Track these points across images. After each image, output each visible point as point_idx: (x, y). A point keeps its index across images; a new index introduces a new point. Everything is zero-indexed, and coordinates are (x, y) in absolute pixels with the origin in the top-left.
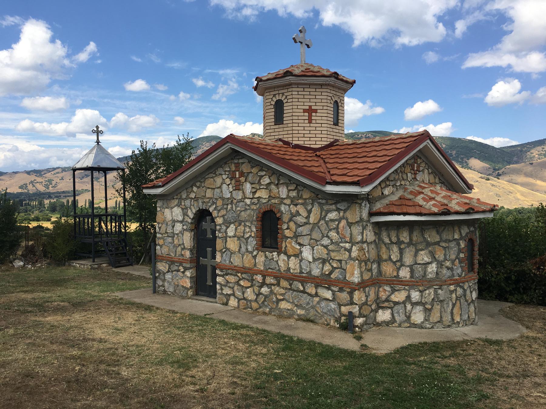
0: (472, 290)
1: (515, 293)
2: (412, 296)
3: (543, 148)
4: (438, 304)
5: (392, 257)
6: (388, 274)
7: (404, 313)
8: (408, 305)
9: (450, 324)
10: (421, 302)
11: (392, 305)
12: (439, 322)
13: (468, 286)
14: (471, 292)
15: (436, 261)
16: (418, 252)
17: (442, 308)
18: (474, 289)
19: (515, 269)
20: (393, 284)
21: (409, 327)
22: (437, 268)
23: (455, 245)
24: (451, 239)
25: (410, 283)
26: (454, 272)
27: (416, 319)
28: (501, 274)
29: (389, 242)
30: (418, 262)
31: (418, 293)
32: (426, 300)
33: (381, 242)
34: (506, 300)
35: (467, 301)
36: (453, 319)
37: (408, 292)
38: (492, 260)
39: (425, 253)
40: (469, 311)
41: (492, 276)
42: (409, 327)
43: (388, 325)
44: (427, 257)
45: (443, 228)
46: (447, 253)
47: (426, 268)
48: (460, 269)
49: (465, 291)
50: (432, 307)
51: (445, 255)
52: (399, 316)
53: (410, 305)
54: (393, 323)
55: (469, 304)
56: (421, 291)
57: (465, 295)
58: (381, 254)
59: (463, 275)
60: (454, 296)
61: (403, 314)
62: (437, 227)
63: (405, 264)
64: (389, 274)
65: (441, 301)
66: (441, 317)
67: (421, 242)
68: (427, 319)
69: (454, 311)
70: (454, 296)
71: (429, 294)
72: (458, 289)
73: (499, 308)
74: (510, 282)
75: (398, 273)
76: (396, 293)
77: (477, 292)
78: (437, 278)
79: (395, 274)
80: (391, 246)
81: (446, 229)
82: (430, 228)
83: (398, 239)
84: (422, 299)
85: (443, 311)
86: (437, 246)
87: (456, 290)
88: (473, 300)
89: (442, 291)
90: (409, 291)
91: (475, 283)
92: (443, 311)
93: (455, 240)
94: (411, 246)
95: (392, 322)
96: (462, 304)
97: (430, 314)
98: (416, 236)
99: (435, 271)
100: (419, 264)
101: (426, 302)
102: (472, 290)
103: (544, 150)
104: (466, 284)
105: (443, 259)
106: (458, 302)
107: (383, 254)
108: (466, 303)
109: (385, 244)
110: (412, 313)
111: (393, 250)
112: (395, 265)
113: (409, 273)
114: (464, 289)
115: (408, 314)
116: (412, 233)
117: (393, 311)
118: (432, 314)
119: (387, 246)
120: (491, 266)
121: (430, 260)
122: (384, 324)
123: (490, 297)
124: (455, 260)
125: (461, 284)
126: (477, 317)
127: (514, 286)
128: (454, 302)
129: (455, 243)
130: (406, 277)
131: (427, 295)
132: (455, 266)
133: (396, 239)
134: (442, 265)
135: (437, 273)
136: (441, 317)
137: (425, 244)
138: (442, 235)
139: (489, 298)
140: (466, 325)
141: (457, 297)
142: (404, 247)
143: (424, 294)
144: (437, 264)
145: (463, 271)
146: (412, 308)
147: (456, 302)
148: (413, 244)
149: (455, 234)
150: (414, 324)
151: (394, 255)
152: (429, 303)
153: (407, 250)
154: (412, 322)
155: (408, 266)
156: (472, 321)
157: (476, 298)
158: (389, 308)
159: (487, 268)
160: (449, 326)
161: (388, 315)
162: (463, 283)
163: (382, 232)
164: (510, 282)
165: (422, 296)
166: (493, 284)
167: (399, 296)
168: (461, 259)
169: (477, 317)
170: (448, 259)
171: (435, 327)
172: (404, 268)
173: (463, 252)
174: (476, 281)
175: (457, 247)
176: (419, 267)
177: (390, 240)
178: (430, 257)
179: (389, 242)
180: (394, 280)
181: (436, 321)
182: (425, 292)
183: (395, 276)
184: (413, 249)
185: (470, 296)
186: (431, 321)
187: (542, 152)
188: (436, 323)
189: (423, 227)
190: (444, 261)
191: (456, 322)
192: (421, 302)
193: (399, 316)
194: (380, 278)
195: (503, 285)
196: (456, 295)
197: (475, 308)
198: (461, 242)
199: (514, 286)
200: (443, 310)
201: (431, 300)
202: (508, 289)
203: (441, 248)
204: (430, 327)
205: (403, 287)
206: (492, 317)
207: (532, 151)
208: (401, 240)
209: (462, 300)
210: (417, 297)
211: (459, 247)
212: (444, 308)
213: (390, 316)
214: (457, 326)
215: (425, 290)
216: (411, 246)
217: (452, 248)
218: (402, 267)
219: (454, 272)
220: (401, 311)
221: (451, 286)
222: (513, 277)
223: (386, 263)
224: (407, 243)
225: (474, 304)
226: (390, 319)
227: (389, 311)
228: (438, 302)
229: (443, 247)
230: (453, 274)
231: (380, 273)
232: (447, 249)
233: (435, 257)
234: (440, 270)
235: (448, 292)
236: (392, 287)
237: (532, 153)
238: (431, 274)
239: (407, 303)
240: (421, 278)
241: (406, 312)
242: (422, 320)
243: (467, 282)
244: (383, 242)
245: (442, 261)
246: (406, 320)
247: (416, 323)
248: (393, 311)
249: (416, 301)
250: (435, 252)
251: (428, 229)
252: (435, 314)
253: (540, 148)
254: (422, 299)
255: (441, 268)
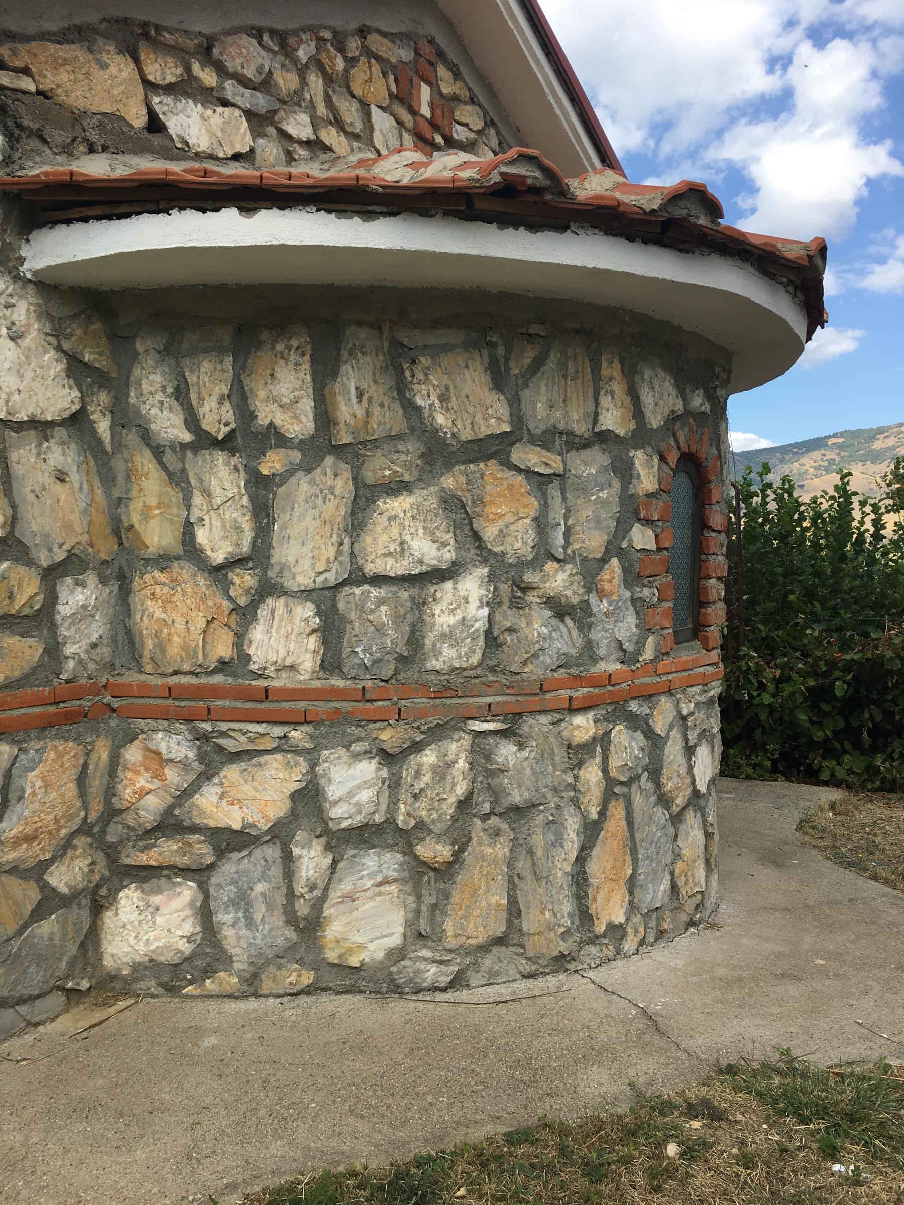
0: (692, 736)
1: (844, 751)
2: (333, 791)
3: (824, 455)
4: (497, 833)
5: (202, 536)
6: (174, 650)
7: (280, 899)
8: (308, 845)
9: (563, 947)
10: (390, 821)
11: (203, 851)
12: (500, 941)
13: (671, 717)
14: (689, 750)
15: (485, 561)
16: (371, 500)
17: (522, 853)
18: (703, 734)
19: (848, 657)
20: (209, 715)
21: (307, 991)
22: (494, 603)
23: (603, 470)
24: (581, 429)
25: (322, 707)
26: (596, 635)
27: (359, 939)
28: (795, 676)
29: (187, 437)
30: (370, 569)
31: (368, 769)
32: (422, 810)
33: (131, 438)
34: (812, 777)
35: (664, 800)
36: (585, 916)
37: (304, 766)
38: (761, 627)
39: (418, 507)
40: (677, 856)
41: (762, 687)
42: (307, 991)
43: (172, 990)
44: (431, 533)
45: (528, 356)
46: (557, 512)
47: (420, 605)
48: (631, 619)
49: (655, 742)
50: (457, 854)
51: (541, 524)
52: (249, 922)
53: (318, 847)
54: (208, 972)
55: (677, 819)
56: (388, 757)
57: (655, 771)
58: (135, 519)
59: (648, 654)
60: (592, 774)
61: (270, 908)
62: (492, 345)
63: (291, 585)
64: (185, 647)
65: (518, 812)
66: (514, 910)
67: (391, 438)
68: (424, 926)
69: (593, 867)
70: (592, 774)
71: (442, 771)
72: (620, 733)
73: (797, 816)
74: (825, 707)
75: (240, 639)
76: (231, 773)
77: (719, 749)
78: (493, 670)
79: (223, 648)
80: (195, 465)
81: (551, 364)
82: (446, 348)
83: (246, 414)
84: (394, 802)
85: (527, 873)
86: (491, 469)
87: (604, 740)
88: (696, 793)
89: (521, 746)
90: (312, 756)
91: (710, 703)
92: (527, 873)
93: (603, 438)
94: (329, 460)
95: (200, 963)
96: (638, 819)
97: (447, 896)
98: (360, 395)
99: (480, 625)
100: (378, 580)
101: (421, 826)
102: (692, 736)
103: (825, 458)
104: (665, 703)
105: (527, 552)
106: (617, 811)
107: (146, 516)
108: (661, 815)
109: (158, 452)
110: (335, 895)
111: (207, 493)
112: (225, 586)
113: (313, 642)
114: (649, 734)
115: (302, 909)
116: (335, 374)
117: (207, 896)
118: (456, 897)
119: (169, 458)
120: (756, 651)
121: (449, 555)
122: (151, 984)
123: (755, 766)
124: (604, 561)
125: (634, 706)
126: (715, 878)
127: (841, 724)
128: (594, 813)
129: (605, 460)
130: (292, 667)
131: (427, 778)
132: (601, 594)
133: (228, 413)
134: (526, 589)
135: (491, 640)
136: (514, 910)
137: (413, 447)
138: (526, 394)
139: (750, 771)
140: (661, 934)
141: (610, 782)
142: (279, 468)
143: (407, 775)
144: (492, 578)
145: (646, 629)
146: (335, 863)
147: (602, 813)
148: (339, 450)
149: (605, 401)
150: (341, 968)
151: (217, 523)
152: (438, 828)
153: (302, 486)
154: (332, 956)
155: (307, 594)
156: (689, 906)
157: (712, 782)
158: (185, 872)
159: (742, 658)
160: (561, 962)
161: (176, 918)
162: (649, 697)
163: (137, 371)
164: (825, 707)
165: (394, 785)
166: (763, 717)
167: (247, 790)
168: (635, 556)
169: (715, 878)
170: (559, 553)
171: (475, 979)
172: (279, 604)
173: (648, 522)
174: (716, 689)
175: (617, 484)
176: (380, 602)
177: (192, 422)
178: (449, 537)
179: (187, 437)
180: (216, 692)
181: (481, 939)
182: (414, 760)
183: (223, 665)
184: (339, 483)
185: (683, 770)
186: (452, 943)
187: (823, 464)
188: (483, 949)
189: (404, 336)
190: (536, 564)
191: (600, 928)
192: (390, 821)
193: (249, 922)
194: (132, 678)
195: (802, 717)
196: (605, 770)
197: (708, 836)
198: (639, 457)
199: (841, 724)
200: (523, 865)
201: (449, 808)
202: (818, 735)
203: (520, 479)
204: (444, 980)
205: (278, 731)
206: (778, 865)
207: (802, 461)
208: (263, 419)
209: (638, 800)
210: (365, 796)
211: (625, 488)
212: (531, 852)
213: (189, 927)
214: (610, 952)
215: (417, 747)
216: (329, 460)
217: (583, 490)
218: (270, 601)
219: (596, 635)
220: (260, 887)
221: (579, 720)
222: (840, 689)
223: (162, 577)
224: (302, 445)
225: (703, 816)
226: (186, 948)
227: (188, 891)
228: (494, 821)
229: (529, 473)
230: (589, 645)
231: (131, 642)
232: (554, 491)
233: (476, 536)
234: (507, 618)
235: (560, 755)
236: (202, 737)
237: (802, 465)
238: (456, 643)
239: (300, 836)
240: (387, 671)
241: (291, 895)
242: (396, 940)
243: (670, 692)
244: (146, 436)
245: (522, 565)
246: (292, 947)
247: (354, 961)
248: (207, 896)
249: (358, 820)
250: (479, 500)
251: (437, 351)
252: (474, 894)
253: (816, 455)
254: (394, 802)
255: (517, 604)
